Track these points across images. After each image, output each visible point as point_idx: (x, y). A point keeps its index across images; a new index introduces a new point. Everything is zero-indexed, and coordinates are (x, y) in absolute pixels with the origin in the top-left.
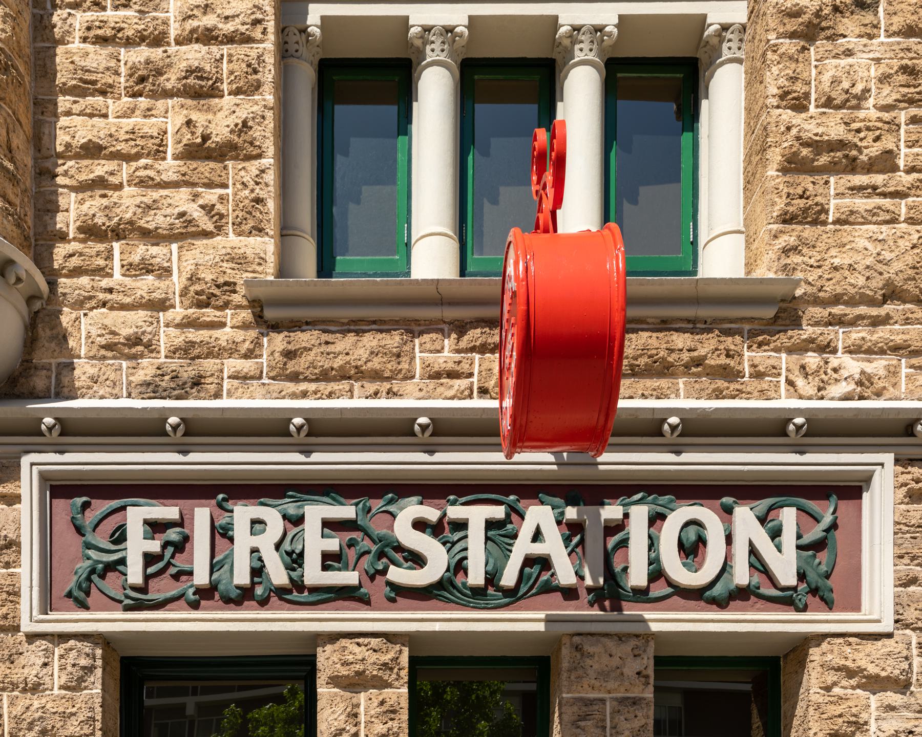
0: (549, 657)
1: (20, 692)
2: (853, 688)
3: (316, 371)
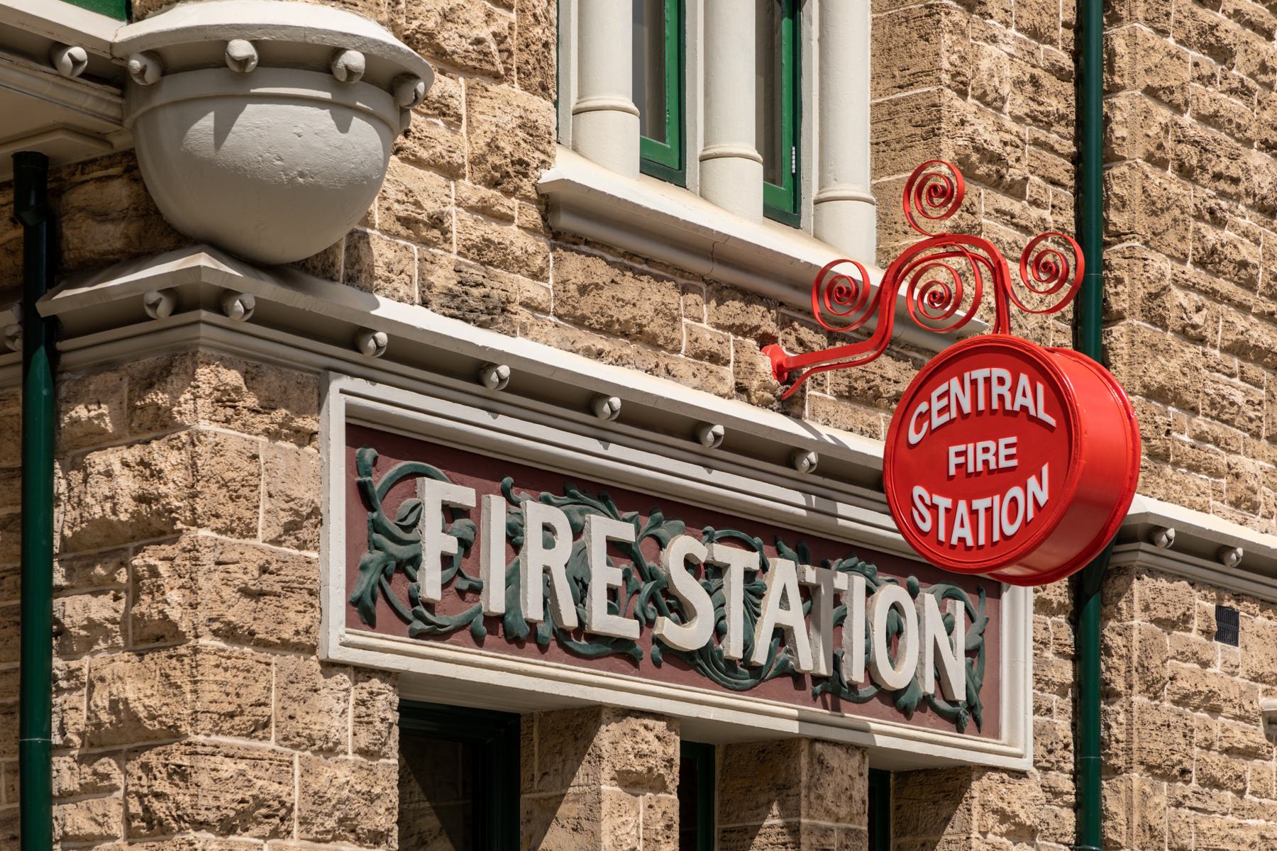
0: (713, 747)
1: (314, 752)
2: (1002, 835)
3: (603, 320)
